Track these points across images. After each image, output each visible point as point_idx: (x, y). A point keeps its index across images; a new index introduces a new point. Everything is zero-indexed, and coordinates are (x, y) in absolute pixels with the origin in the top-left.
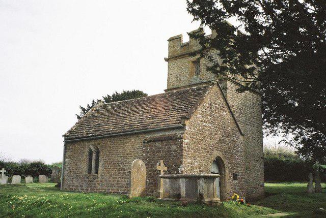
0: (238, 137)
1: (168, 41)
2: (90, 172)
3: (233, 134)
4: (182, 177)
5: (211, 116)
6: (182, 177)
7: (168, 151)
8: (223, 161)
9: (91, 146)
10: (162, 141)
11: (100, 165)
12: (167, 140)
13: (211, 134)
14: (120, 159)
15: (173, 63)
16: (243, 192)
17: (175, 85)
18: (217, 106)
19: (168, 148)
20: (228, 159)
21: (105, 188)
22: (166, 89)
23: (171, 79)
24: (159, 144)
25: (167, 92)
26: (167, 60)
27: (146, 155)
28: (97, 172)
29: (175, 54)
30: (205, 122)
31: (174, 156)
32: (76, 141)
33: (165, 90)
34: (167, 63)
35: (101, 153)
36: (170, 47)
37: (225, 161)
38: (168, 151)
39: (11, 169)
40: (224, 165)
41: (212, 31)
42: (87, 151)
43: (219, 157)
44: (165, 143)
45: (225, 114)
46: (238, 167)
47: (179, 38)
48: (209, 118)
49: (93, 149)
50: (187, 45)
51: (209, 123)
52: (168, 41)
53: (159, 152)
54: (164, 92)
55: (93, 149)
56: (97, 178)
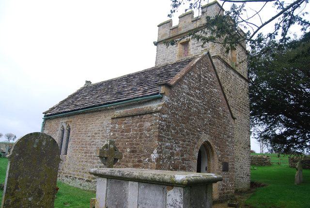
0: (229, 121)
5: (199, 89)
7: (140, 131)
8: (211, 147)
10: (133, 116)
12: (140, 115)
13: (199, 112)
14: (88, 139)
15: (163, 46)
16: (232, 184)
18: (207, 79)
19: (141, 126)
20: (217, 145)
21: (71, 172)
24: (129, 121)
26: (156, 44)
27: (114, 135)
30: (192, 95)
36: (159, 30)
37: (215, 147)
38: (140, 131)
40: (212, 151)
43: (207, 142)
44: (136, 119)
45: (216, 91)
46: (228, 155)
49: (65, 127)
51: (197, 97)
53: (128, 131)
55: (65, 127)
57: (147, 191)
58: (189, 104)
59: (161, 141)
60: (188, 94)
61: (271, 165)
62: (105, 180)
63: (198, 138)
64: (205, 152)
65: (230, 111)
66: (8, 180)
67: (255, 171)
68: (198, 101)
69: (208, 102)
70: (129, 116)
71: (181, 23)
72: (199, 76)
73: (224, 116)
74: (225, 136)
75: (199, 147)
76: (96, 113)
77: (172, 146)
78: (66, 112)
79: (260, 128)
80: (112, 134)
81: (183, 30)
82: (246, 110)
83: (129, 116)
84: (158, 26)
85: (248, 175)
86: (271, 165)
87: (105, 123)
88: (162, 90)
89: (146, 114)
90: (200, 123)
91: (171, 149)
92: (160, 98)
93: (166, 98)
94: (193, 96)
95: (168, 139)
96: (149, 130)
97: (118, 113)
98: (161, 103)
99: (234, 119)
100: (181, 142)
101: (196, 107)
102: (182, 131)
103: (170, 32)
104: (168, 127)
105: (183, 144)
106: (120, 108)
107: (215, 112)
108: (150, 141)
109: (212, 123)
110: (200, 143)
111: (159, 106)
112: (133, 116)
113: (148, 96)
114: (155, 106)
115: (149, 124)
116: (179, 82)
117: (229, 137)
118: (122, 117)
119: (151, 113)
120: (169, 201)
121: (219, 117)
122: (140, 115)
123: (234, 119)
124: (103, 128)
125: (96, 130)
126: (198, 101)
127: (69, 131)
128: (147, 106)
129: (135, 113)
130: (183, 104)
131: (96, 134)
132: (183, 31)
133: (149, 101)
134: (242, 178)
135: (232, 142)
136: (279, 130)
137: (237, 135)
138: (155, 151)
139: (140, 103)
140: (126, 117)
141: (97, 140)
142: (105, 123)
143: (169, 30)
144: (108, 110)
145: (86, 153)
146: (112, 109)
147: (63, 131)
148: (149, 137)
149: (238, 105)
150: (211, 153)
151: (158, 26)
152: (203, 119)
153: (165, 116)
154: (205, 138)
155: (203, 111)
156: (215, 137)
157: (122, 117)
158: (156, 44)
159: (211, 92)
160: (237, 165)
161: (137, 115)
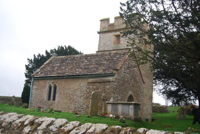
0: (142, 84)
1: (100, 21)
2: (49, 99)
3: (139, 82)
4: (110, 103)
6: (110, 103)
7: (104, 89)
9: (50, 83)
10: (100, 83)
11: (57, 96)
12: (104, 82)
13: (128, 81)
17: (101, 49)
18: (132, 64)
19: (104, 87)
22: (97, 51)
23: (102, 44)
24: (98, 85)
25: (98, 53)
26: (99, 33)
27: (89, 91)
28: (54, 99)
29: (105, 30)
31: (107, 92)
32: (46, 79)
33: (97, 52)
34: (99, 34)
35: (58, 88)
36: (101, 24)
37: (134, 97)
38: (104, 89)
39: (198, 132)
41: (115, 21)
42: (48, 86)
43: (131, 95)
44: (102, 84)
47: (108, 20)
48: (128, 71)
49: (52, 85)
50: (112, 25)
52: (100, 21)
53: (98, 89)
54: (96, 53)
56: (55, 104)
57: (124, 106)
58: (125, 77)
59: (114, 94)
60: (124, 72)
61: (168, 112)
62: (111, 105)
63: (127, 93)
64: (131, 98)
65: (142, 79)
66: (91, 104)
67: (157, 116)
68: (128, 75)
69: (132, 75)
70: (98, 82)
71: (116, 22)
72: (129, 63)
73: (139, 82)
74: (139, 92)
75: (128, 97)
76: (75, 79)
77: (118, 96)
78: (60, 76)
79: (159, 86)
80: (88, 90)
81: (117, 27)
82: (151, 77)
83: (98, 82)
84: (100, 21)
85: (150, 114)
86: (168, 112)
87: (82, 85)
88: (114, 72)
89: (107, 82)
90: (128, 86)
91: (117, 98)
92: (113, 76)
93: (116, 75)
94: (126, 73)
95: (117, 93)
96: (108, 89)
97: (90, 80)
98: (114, 78)
99: (144, 83)
100: (121, 95)
101: (127, 79)
102: (121, 90)
103: (108, 27)
104: (117, 88)
105: (122, 96)
106: (91, 78)
107: (135, 80)
108: (110, 94)
109: (133, 86)
110: (128, 95)
111: (113, 79)
112: (100, 83)
113: (107, 74)
114: (111, 79)
115: (109, 87)
116: (121, 67)
117: (141, 93)
118: (94, 83)
119: (109, 82)
120: (130, 108)
121: (137, 83)
122: (104, 82)
123: (144, 83)
124: (81, 87)
125: (76, 88)
126: (128, 75)
127: (55, 88)
128: (107, 78)
129: (101, 81)
130: (122, 77)
131: (76, 90)
132: (117, 28)
133: (108, 76)
134: (147, 115)
135: (142, 95)
136: (173, 89)
137: (145, 91)
138: (112, 98)
139: (103, 77)
140: (96, 82)
141: (77, 93)
142: (82, 85)
143: (108, 26)
144: (84, 78)
145: (69, 99)
146: (87, 78)
147: (50, 88)
148: (109, 92)
149: (147, 74)
150: (132, 99)
151: (100, 21)
152: (130, 84)
153: (116, 83)
154: (130, 93)
155: (130, 80)
156: (135, 93)
157: (94, 83)
158: (99, 33)
159: (134, 70)
160: (145, 108)
161: (102, 82)
